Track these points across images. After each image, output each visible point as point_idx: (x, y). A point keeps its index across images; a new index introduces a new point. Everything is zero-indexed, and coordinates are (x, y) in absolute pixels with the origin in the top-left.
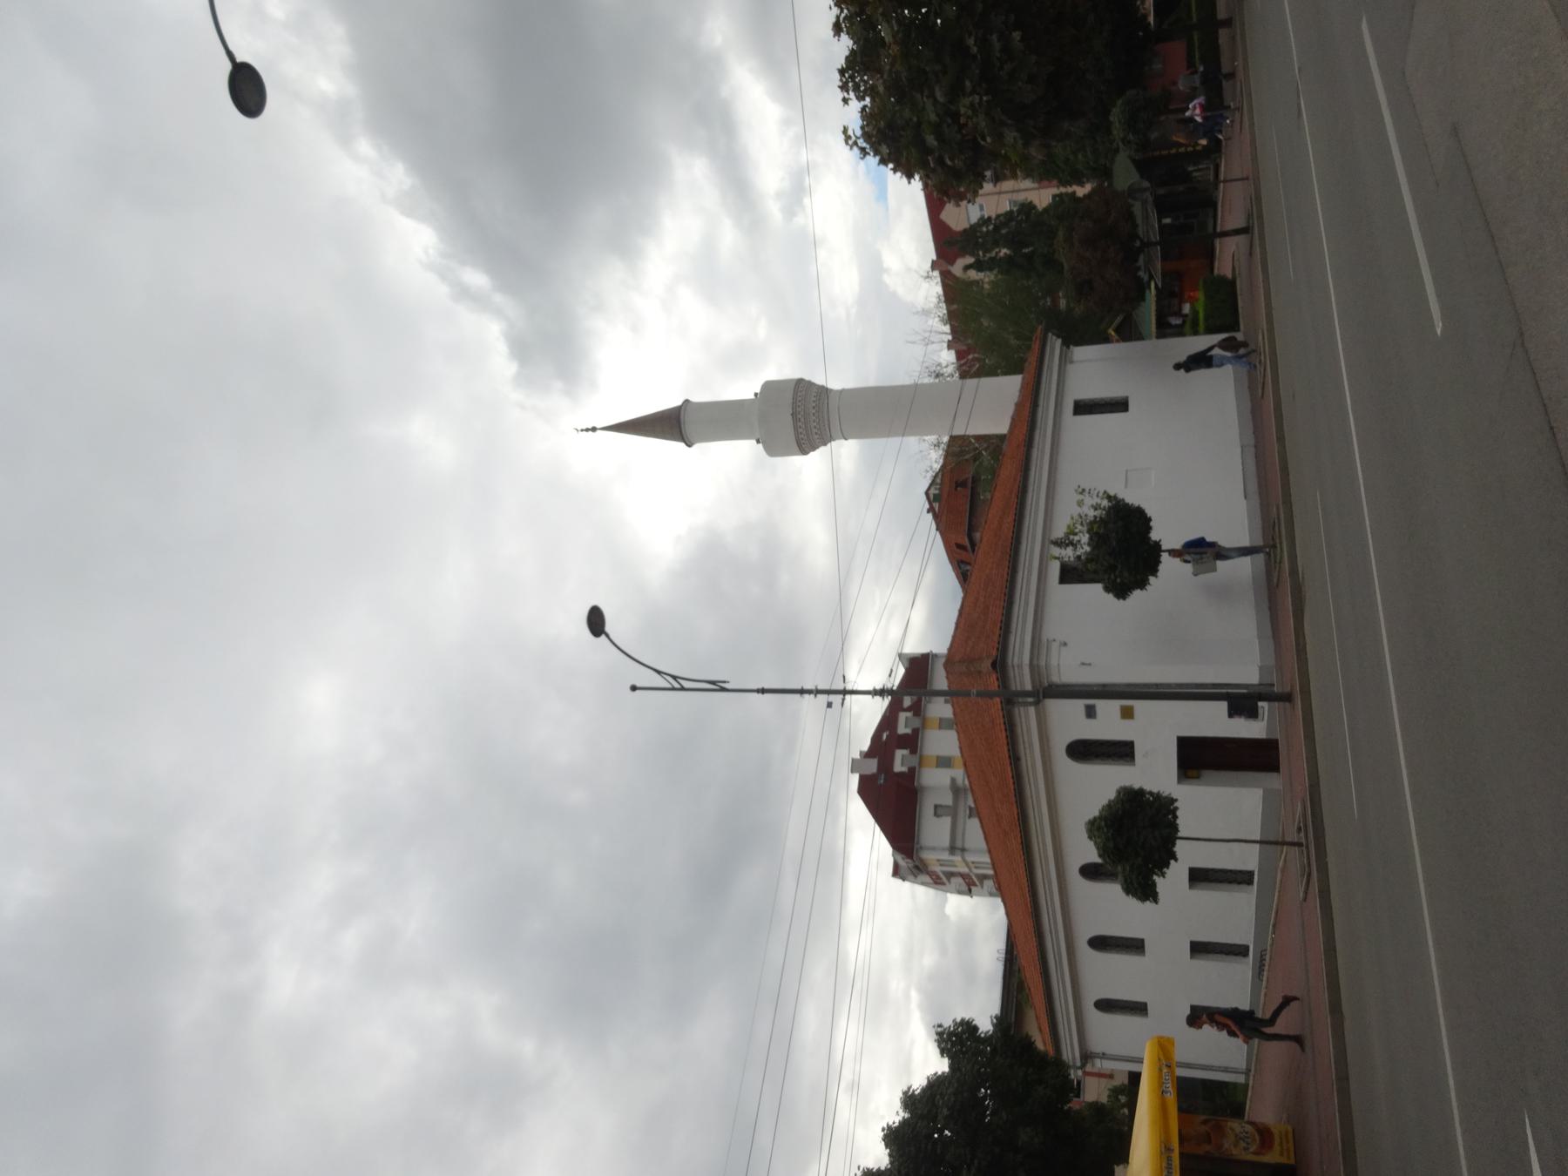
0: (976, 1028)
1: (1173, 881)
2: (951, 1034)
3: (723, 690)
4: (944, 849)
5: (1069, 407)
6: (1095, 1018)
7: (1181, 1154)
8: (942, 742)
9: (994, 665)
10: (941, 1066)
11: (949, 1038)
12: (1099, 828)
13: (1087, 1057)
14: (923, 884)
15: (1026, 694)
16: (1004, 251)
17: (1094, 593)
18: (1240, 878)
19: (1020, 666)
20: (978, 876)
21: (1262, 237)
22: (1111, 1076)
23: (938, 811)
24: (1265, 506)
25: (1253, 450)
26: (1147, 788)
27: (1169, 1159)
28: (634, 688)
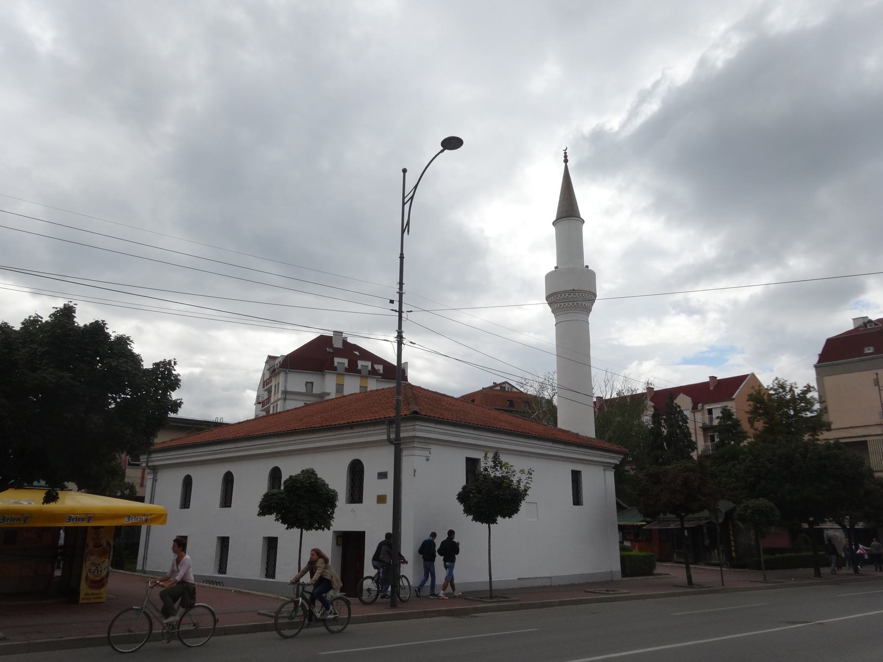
0: (174, 389)
1: (272, 525)
2: (170, 371)
3: (403, 232)
4: (285, 387)
6: (181, 474)
7: (87, 527)
8: (352, 385)
9: (416, 412)
10: (147, 365)
11: (166, 369)
12: (310, 477)
13: (155, 469)
14: (264, 374)
15: (398, 433)
16: (665, 431)
17: (460, 481)
18: (270, 568)
19: (414, 430)
20: (269, 407)
21: (687, 594)
22: (142, 485)
23: (310, 384)
24: (514, 591)
25: (549, 584)
26: (336, 510)
27: (83, 519)
28: (405, 171)
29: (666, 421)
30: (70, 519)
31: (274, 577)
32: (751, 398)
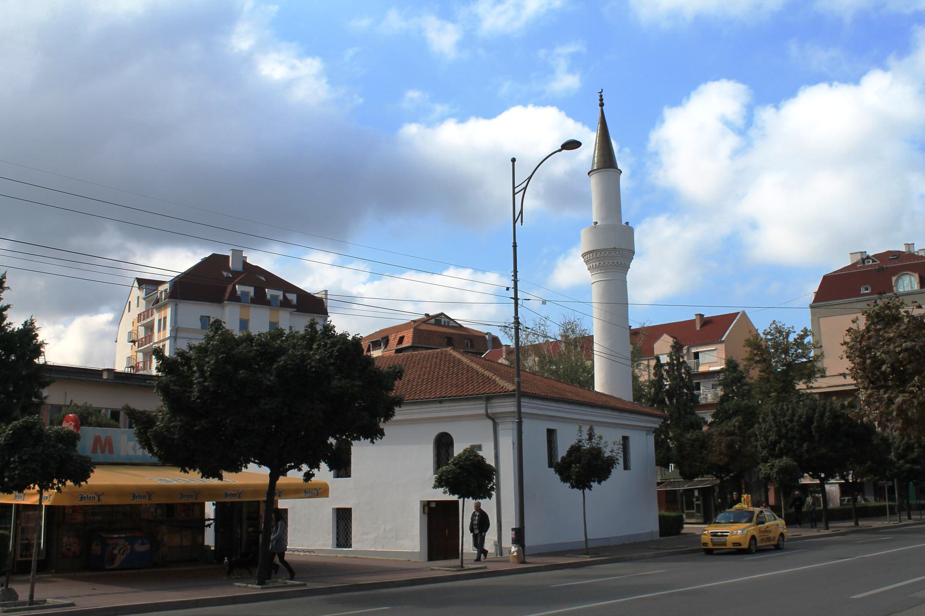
5: (552, 426)
27: (235, 495)
28: (514, 160)
29: (668, 372)
30: (227, 495)
31: (350, 546)
32: (749, 343)
